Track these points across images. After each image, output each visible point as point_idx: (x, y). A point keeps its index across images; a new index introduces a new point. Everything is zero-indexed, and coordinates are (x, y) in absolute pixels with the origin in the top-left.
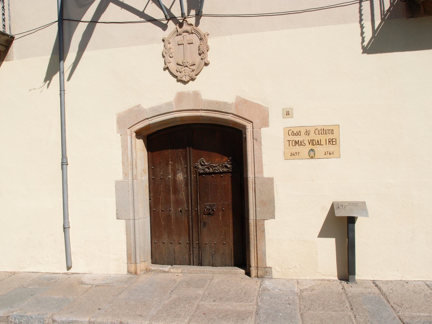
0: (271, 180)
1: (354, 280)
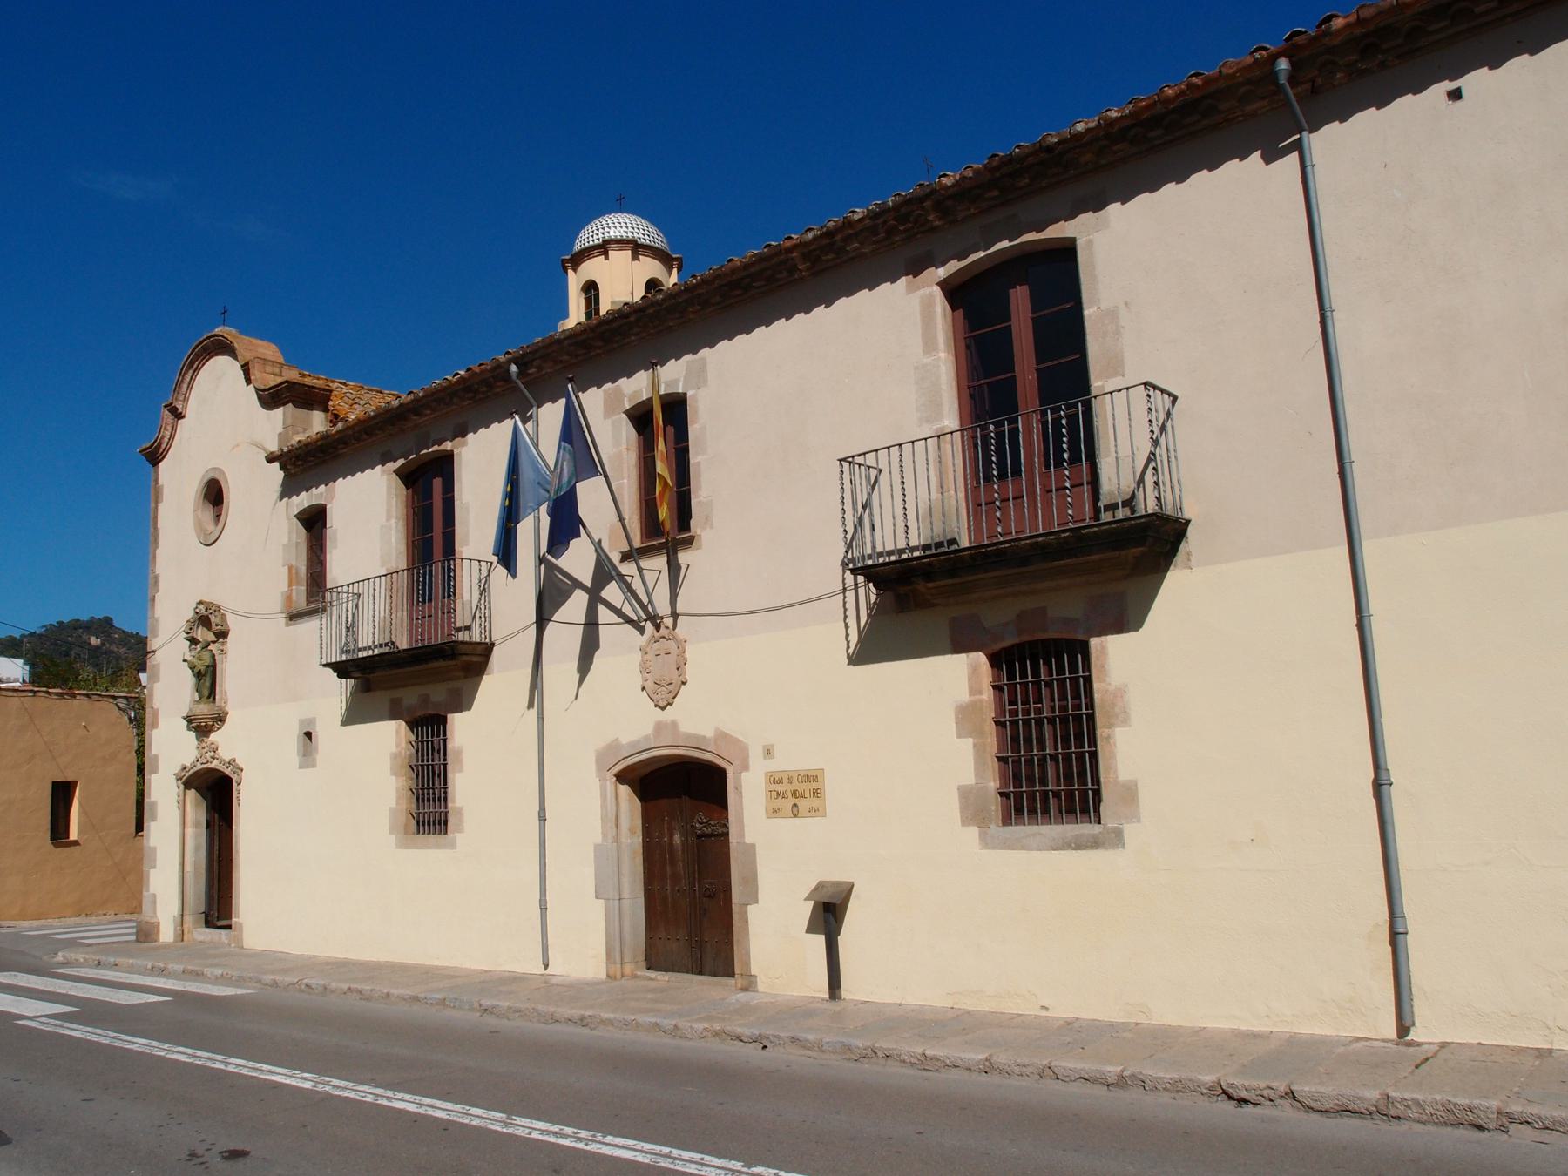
0: (753, 846)
1: (840, 998)
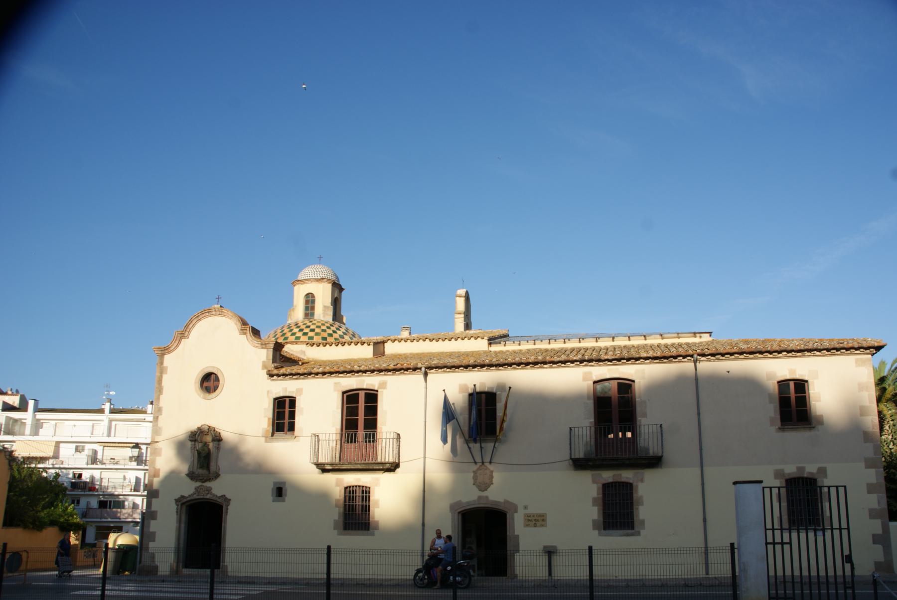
0: (518, 536)
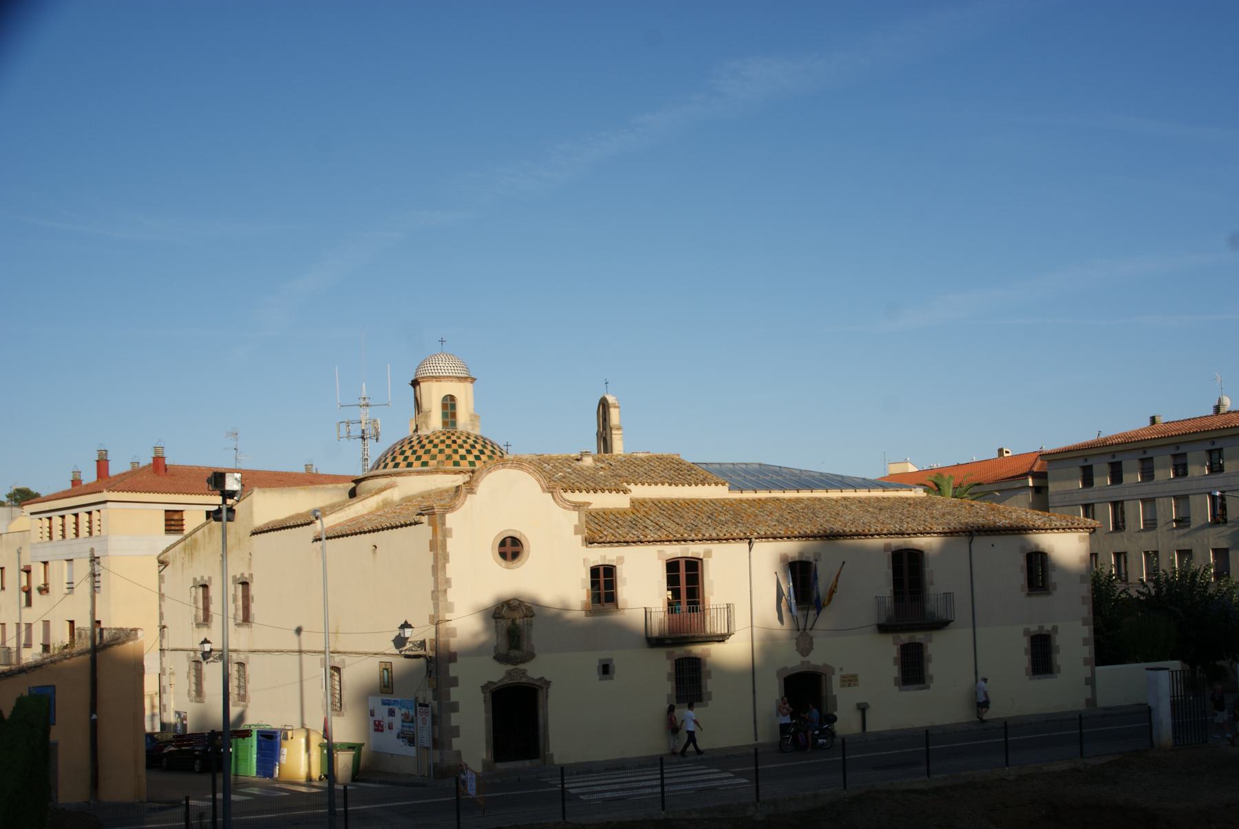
0: (835, 696)
